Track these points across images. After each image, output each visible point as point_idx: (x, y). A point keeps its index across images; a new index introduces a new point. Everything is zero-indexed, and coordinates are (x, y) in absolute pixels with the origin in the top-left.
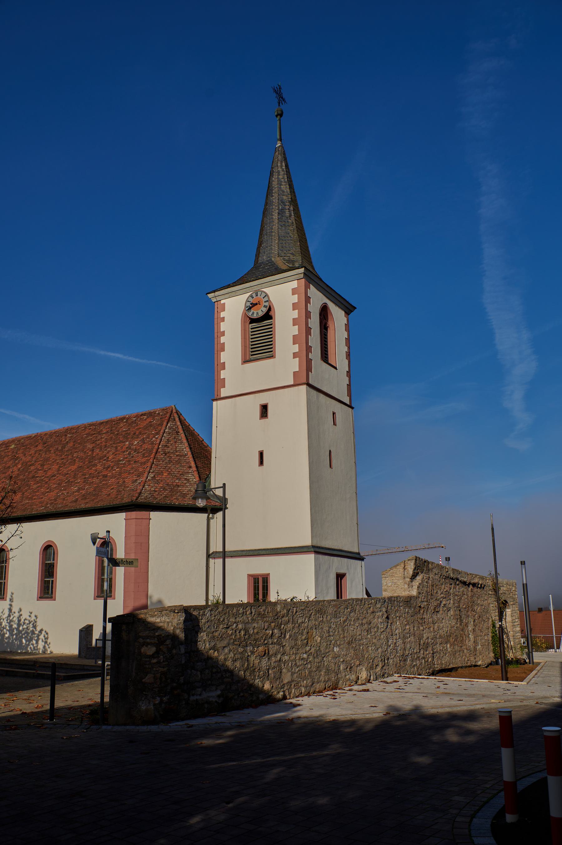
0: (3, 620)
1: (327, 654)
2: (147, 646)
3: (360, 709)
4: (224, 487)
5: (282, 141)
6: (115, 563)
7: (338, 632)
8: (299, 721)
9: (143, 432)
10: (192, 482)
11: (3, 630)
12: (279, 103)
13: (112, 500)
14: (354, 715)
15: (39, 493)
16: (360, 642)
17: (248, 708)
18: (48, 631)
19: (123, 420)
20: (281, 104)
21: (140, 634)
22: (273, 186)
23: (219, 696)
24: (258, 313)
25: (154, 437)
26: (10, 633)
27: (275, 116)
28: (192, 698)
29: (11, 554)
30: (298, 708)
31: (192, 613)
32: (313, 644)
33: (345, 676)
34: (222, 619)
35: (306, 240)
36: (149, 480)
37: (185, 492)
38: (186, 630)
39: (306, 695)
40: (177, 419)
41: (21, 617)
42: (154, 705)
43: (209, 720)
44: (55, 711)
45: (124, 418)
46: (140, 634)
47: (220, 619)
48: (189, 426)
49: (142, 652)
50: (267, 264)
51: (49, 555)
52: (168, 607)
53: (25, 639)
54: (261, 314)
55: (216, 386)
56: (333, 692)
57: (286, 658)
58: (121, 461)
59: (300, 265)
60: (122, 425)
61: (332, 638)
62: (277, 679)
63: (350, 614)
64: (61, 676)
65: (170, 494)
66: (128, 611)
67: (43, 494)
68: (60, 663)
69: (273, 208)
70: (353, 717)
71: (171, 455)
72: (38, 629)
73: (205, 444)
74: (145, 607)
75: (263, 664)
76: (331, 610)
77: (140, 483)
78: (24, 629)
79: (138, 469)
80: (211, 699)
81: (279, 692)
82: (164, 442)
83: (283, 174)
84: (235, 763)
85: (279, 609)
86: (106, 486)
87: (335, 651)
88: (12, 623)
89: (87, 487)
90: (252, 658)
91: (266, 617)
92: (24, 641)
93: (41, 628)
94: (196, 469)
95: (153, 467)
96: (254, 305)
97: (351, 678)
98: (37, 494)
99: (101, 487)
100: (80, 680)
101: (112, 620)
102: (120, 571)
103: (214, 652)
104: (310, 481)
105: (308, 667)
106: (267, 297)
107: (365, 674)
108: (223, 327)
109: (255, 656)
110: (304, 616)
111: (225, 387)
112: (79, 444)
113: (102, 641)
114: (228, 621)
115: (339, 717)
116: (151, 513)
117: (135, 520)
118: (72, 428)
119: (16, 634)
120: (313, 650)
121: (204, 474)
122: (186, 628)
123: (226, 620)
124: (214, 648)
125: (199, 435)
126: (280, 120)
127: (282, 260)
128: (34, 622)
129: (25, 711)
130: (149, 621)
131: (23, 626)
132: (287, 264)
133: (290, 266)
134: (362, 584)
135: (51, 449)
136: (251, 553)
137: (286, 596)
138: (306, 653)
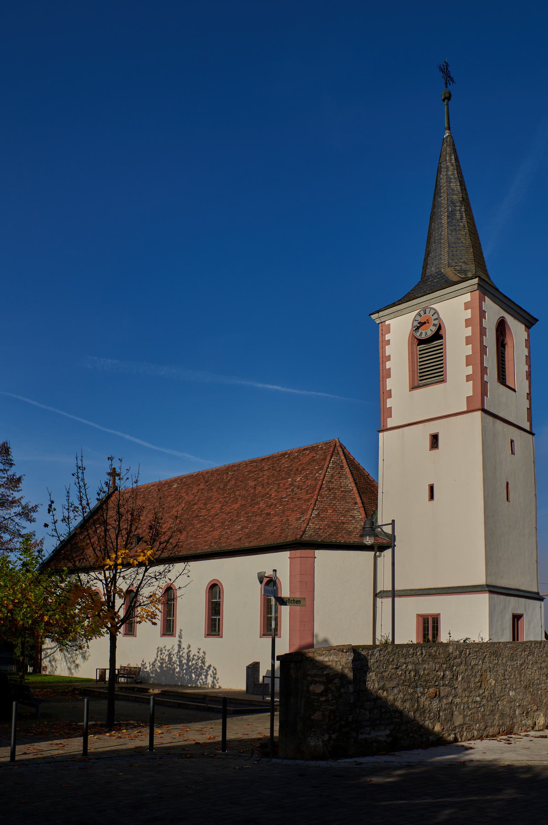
0: (174, 655)
1: (502, 698)
2: (315, 684)
3: (537, 755)
4: (393, 524)
5: (451, 129)
6: (282, 601)
7: (515, 675)
8: (471, 764)
9: (305, 468)
10: (357, 519)
11: (174, 665)
12: (446, 84)
13: (276, 538)
14: (531, 762)
15: (203, 532)
16: (538, 687)
17: (417, 749)
18: (215, 667)
19: (285, 456)
20: (448, 84)
21: (308, 672)
22: (441, 184)
23: (388, 736)
24: (426, 333)
25: (318, 472)
26: (180, 668)
27: (442, 101)
28: (361, 737)
29: (179, 593)
30: (470, 751)
31: (360, 653)
32: (487, 687)
33: (521, 721)
34: (391, 660)
35: (480, 245)
36: (313, 518)
37: (351, 530)
38: (355, 669)
39: (479, 739)
40: (341, 453)
41: (190, 653)
42: (323, 741)
43: (378, 758)
44: (227, 742)
45: (286, 454)
46: (308, 672)
47: (389, 659)
48: (354, 460)
49: (311, 690)
50: (436, 276)
51: (215, 594)
52: (336, 646)
53: (194, 674)
54: (430, 334)
55: (382, 416)
56: (508, 737)
57: (458, 700)
58: (284, 498)
59: (473, 274)
60: (284, 461)
61: (508, 681)
62: (449, 721)
63: (528, 657)
64: (230, 710)
65: (335, 531)
66: (294, 649)
67: (208, 533)
68: (229, 698)
69: (441, 211)
70: (530, 763)
71: (335, 492)
72: (207, 664)
73: (370, 478)
74: (311, 646)
75: (434, 706)
76: (506, 652)
77: (304, 521)
78: (193, 664)
79: (301, 506)
80: (380, 738)
81: (450, 735)
82: (328, 478)
83: (452, 169)
84: (414, 802)
85: (451, 650)
86: (270, 524)
87: (511, 695)
88: (182, 659)
89: (251, 525)
90: (423, 699)
91: (437, 658)
92: (193, 676)
93: (209, 664)
94: (362, 506)
95: (317, 504)
96: (422, 324)
97: (528, 723)
98: (201, 533)
99: (264, 525)
100: (249, 715)
101: (280, 658)
102: (285, 610)
103: (383, 692)
104: (484, 516)
105: (481, 711)
106: (436, 314)
107: (543, 720)
108: (389, 350)
109: (425, 697)
110: (478, 658)
111: (391, 417)
112: (241, 481)
113: (270, 678)
114: (398, 661)
115: (514, 763)
116: (316, 551)
117: (299, 559)
118: (233, 466)
119: (186, 669)
120: (486, 693)
121: (370, 510)
122: (354, 667)
123: (395, 660)
124: (383, 688)
125: (364, 469)
126: (448, 104)
127: (453, 271)
128: (202, 658)
129: (198, 742)
130: (318, 660)
131: (192, 662)
132: (458, 274)
133: (462, 277)
134: (541, 626)
135: (213, 487)
136: (421, 592)
137: (458, 636)
138: (479, 696)
